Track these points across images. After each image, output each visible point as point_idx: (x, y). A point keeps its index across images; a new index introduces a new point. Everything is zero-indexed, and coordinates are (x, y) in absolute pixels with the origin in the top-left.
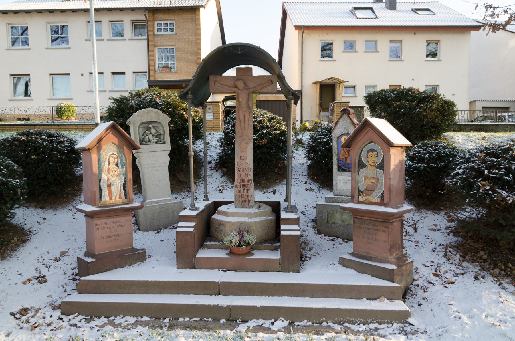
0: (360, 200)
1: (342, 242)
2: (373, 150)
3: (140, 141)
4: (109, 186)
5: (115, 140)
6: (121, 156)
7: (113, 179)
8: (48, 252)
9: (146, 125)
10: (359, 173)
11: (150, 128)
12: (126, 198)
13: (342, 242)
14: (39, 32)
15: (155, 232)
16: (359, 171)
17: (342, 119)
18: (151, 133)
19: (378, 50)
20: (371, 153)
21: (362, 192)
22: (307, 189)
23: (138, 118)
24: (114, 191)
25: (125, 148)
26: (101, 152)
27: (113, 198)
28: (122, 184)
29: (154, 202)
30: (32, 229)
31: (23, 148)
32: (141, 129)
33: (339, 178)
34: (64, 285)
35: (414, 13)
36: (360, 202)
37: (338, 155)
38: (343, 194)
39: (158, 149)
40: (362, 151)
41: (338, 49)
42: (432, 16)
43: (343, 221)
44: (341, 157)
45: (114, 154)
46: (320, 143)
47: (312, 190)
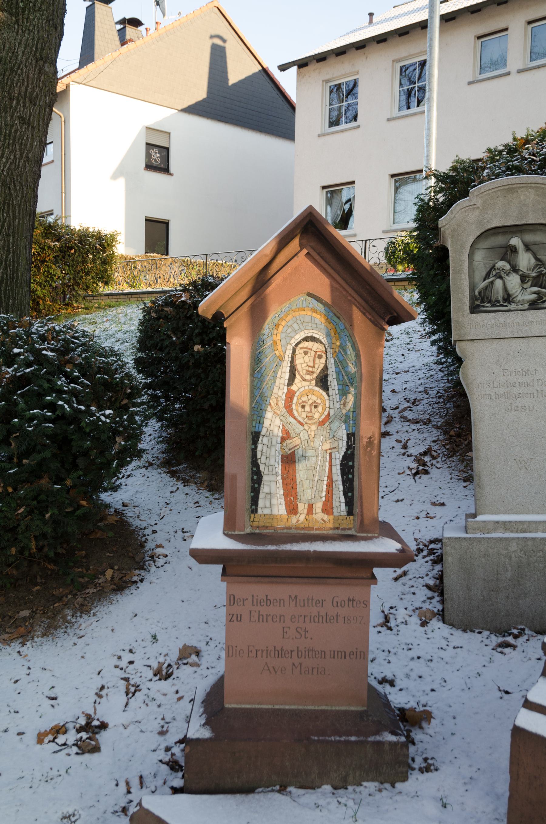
3: (473, 298)
4: (289, 460)
5: (320, 282)
6: (342, 347)
7: (304, 436)
8: (155, 637)
9: (499, 240)
11: (514, 250)
12: (350, 513)
14: (377, 82)
15: (495, 640)
18: (515, 269)
23: (473, 216)
24: (307, 483)
25: (357, 315)
26: (266, 329)
27: (302, 508)
28: (338, 456)
29: (506, 526)
30: (159, 551)
32: (479, 256)
34: (135, 783)
39: (536, 330)
45: (312, 339)
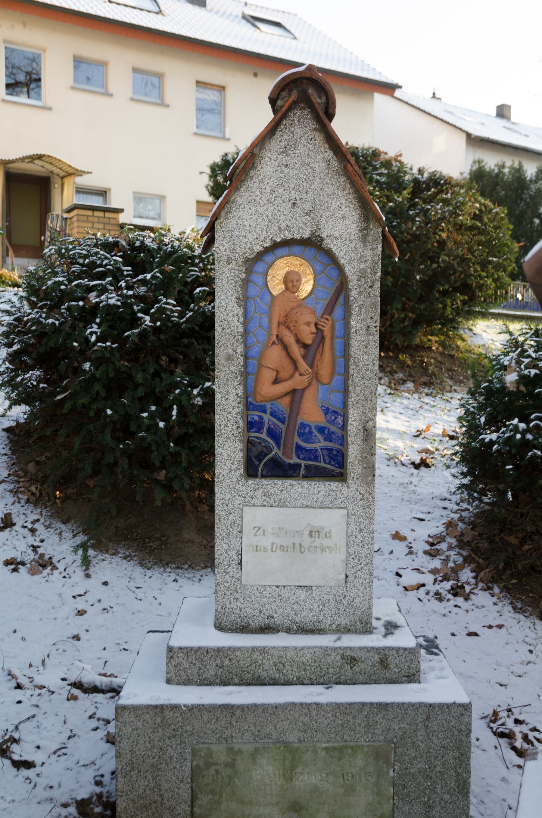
17: (276, 144)
19: (167, 100)
22: (15, 565)
31: (193, 419)
33: (253, 517)
35: (249, 25)
37: (248, 376)
38: (279, 620)
41: (56, 74)
42: (288, 41)
44: (267, 389)
46: (89, 314)
47: (44, 564)
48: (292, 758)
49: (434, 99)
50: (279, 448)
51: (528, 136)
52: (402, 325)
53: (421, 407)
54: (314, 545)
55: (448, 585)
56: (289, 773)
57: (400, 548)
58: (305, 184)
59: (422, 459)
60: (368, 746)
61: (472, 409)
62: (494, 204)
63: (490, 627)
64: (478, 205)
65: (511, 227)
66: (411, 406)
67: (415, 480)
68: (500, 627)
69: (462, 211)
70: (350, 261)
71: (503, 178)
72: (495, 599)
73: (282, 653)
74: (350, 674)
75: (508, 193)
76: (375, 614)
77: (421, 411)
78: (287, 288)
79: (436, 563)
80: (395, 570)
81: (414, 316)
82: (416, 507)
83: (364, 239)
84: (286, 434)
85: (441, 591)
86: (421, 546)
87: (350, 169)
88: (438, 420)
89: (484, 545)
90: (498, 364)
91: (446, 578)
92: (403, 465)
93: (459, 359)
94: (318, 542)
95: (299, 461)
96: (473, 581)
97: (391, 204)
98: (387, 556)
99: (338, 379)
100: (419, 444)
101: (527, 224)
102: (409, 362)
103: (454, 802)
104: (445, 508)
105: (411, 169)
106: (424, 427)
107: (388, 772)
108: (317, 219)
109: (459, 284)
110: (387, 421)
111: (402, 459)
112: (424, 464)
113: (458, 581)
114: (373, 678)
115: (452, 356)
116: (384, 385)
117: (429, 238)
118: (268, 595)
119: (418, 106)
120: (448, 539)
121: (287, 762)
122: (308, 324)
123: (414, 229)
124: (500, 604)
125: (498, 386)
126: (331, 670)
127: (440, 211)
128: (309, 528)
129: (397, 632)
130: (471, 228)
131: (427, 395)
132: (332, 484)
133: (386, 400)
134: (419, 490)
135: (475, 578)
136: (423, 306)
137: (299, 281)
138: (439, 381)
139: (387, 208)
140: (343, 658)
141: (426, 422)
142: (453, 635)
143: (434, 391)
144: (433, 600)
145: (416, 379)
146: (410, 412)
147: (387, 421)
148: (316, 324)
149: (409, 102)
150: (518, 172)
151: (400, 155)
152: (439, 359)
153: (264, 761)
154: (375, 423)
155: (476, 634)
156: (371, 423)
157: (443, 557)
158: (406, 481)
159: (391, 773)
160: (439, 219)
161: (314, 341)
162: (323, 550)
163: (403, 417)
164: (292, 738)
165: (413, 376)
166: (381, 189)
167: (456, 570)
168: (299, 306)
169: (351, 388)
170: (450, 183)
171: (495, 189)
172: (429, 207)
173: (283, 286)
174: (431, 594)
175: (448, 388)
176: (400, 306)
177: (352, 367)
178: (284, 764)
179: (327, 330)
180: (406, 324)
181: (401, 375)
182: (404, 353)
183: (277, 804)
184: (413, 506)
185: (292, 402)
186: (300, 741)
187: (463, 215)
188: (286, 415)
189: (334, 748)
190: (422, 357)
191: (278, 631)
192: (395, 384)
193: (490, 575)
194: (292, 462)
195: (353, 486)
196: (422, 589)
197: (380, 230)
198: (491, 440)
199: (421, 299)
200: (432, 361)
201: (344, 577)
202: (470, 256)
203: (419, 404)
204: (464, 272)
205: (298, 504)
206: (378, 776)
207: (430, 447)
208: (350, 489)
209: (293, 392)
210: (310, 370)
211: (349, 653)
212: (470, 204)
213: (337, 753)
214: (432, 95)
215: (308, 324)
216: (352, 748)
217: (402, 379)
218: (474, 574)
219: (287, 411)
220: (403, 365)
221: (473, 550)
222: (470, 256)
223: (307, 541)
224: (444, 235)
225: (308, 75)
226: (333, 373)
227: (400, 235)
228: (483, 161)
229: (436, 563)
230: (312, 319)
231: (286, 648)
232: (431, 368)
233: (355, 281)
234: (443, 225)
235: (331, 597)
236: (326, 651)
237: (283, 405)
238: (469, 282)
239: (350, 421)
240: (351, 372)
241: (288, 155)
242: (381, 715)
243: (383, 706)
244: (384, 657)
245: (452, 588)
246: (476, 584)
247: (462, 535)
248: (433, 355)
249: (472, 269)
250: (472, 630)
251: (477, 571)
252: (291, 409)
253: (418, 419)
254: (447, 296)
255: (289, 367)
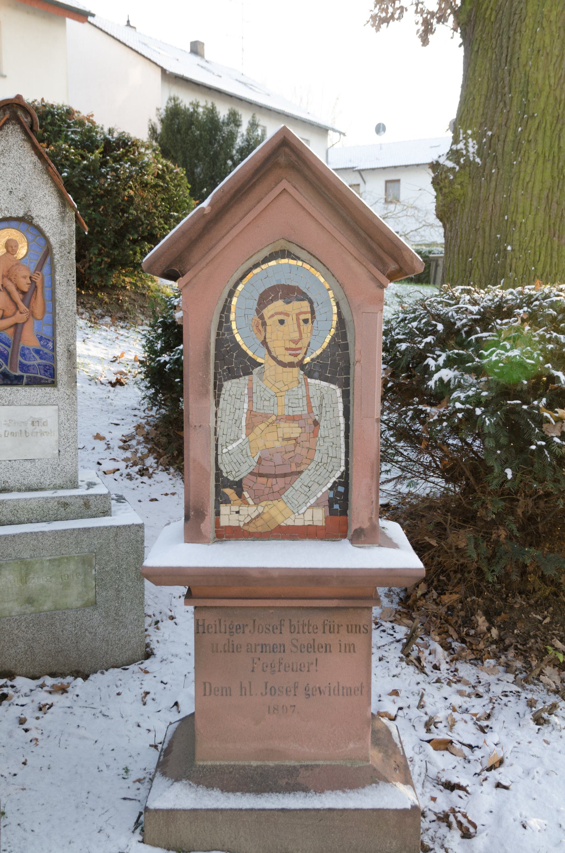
0: (224, 522)
1: (43, 697)
2: (289, 293)
10: (217, 397)
13: (43, 697)
16: (218, 388)
20: (278, 305)
21: (238, 487)
36: (224, 534)
38: (12, 483)
40: (231, 294)
43: (30, 601)
48: (26, 568)
49: (128, 28)
50: (7, 364)
51: (220, 77)
52: (99, 268)
53: (117, 338)
54: (36, 431)
55: (136, 469)
56: (24, 579)
57: (101, 445)
58: (18, 178)
59: (117, 379)
60: (78, 556)
61: (151, 338)
62: (175, 166)
63: (166, 494)
64: (160, 166)
65: (190, 186)
66: (109, 337)
67: (111, 395)
68: (173, 494)
69: (147, 171)
70: (54, 235)
71: (197, 118)
72: (171, 476)
73: (16, 503)
74: (64, 513)
75: (203, 133)
76: (80, 478)
77: (117, 341)
78: (8, 251)
79: (128, 454)
80: (97, 461)
81: (109, 260)
82: (113, 416)
83: (63, 219)
84: (12, 355)
85: (131, 473)
86: (116, 443)
87: (51, 170)
88: (131, 348)
89: (164, 440)
90: (170, 304)
91: (135, 464)
92: (102, 384)
93: (149, 297)
94: (38, 429)
95: (22, 374)
96: (155, 465)
97: (85, 162)
98: (90, 451)
99: (48, 316)
100: (115, 368)
101: (221, 165)
102: (107, 300)
103: (135, 587)
104: (135, 416)
105: (102, 129)
106: (119, 355)
107: (91, 572)
108: (28, 204)
109: (146, 234)
110: (89, 350)
111: (101, 379)
112: (119, 383)
113: (144, 465)
114: (80, 515)
115: (144, 295)
116: (85, 319)
117: (119, 194)
118: (3, 467)
119: (112, 34)
120: (137, 437)
121: (23, 572)
122: (25, 277)
123: (106, 185)
124: (174, 479)
125: (170, 321)
126: (51, 512)
127: (128, 171)
128: (31, 420)
129: (95, 487)
130: (156, 186)
131: (122, 327)
132: (47, 388)
133: (87, 332)
134: (115, 403)
135: (157, 463)
136: (116, 253)
137: (17, 246)
138: (132, 316)
139: (82, 165)
140: (58, 504)
141: (121, 350)
142: (140, 501)
143: (128, 325)
144: (125, 480)
145: (113, 314)
146: (108, 342)
147: (89, 350)
148: (30, 278)
149: (103, 29)
150: (211, 112)
151: (92, 116)
152: (133, 297)
153: (7, 573)
154: (75, 346)
155: (156, 500)
156: (72, 346)
157: (133, 450)
158: (104, 396)
159: (94, 572)
160: (128, 177)
161: (29, 289)
162: (42, 434)
163: (102, 346)
164: (26, 555)
165: (110, 312)
166: (76, 148)
167: (142, 459)
168: (17, 264)
169: (57, 323)
170: (136, 145)
171: (190, 128)
172: (118, 166)
173: (5, 250)
174: (124, 475)
175: (140, 322)
176: (96, 252)
177: (58, 308)
178: (20, 573)
179: (38, 282)
180: (103, 266)
181: (100, 311)
182: (102, 291)
183: (17, 600)
184: (110, 415)
185: (15, 332)
186: (31, 557)
187: (148, 175)
188: (12, 342)
189: (55, 560)
190: (118, 295)
191: (12, 491)
192: (95, 319)
193: (167, 460)
194: (17, 374)
195: (62, 390)
196: (117, 473)
197: (74, 213)
198: (165, 361)
199: (115, 246)
200: (127, 298)
201: (57, 451)
202: (154, 211)
203: (115, 335)
204: (151, 224)
205: (23, 403)
206: (85, 575)
207: (123, 370)
208: (59, 393)
209: (16, 325)
210: (28, 310)
211: (63, 500)
212: (153, 165)
213: (57, 563)
214: (126, 23)
215: (25, 277)
216: (67, 558)
217: (101, 314)
218: (156, 460)
219: (12, 339)
220: (101, 302)
221: (155, 444)
222: (154, 211)
223: (30, 428)
224: (132, 193)
225: (17, 102)
226: (44, 312)
227: (94, 190)
228: (178, 99)
229: (128, 454)
230: (28, 274)
231: (18, 500)
232: (126, 305)
233: (57, 249)
234: (131, 183)
235: (49, 466)
236: (46, 500)
237: (9, 334)
238: (155, 232)
239: (58, 345)
240: (57, 311)
241: (5, 157)
242: (85, 536)
243: (87, 530)
244: (86, 502)
245: (140, 471)
246: (157, 467)
247: (148, 433)
248: (127, 293)
249: (157, 222)
250: (153, 497)
251: (158, 458)
252: (14, 337)
253: (114, 348)
254: (137, 244)
255: (12, 308)
